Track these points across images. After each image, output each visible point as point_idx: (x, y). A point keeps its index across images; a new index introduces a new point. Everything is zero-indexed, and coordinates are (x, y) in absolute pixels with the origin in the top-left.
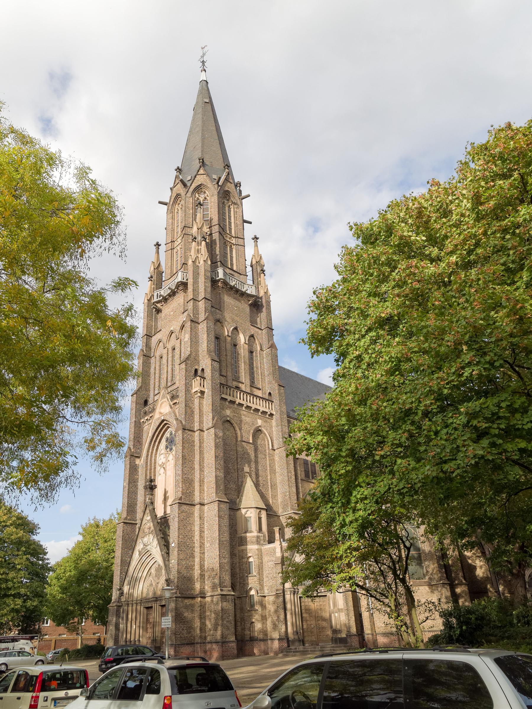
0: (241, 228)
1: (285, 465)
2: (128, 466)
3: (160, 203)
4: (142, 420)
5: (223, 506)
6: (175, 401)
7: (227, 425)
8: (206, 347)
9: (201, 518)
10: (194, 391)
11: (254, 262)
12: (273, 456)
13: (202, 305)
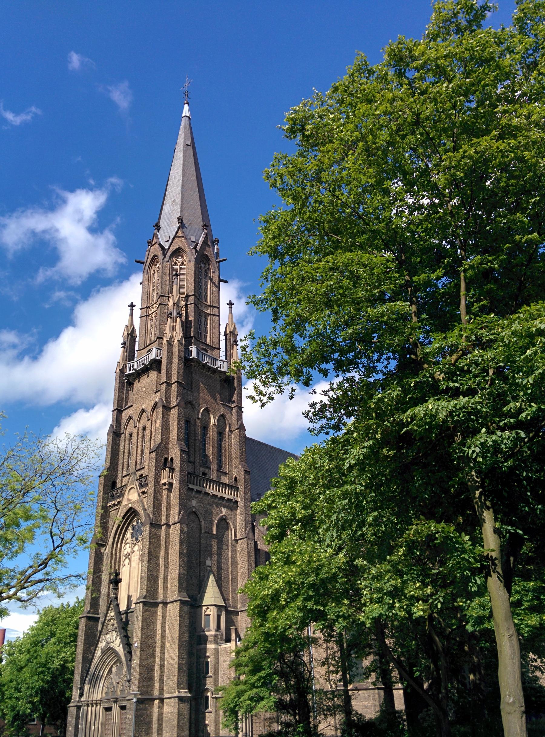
0: (217, 295)
1: (246, 556)
2: (93, 555)
3: (136, 261)
4: (109, 504)
5: (186, 608)
6: (144, 489)
7: (193, 517)
8: (176, 435)
9: (164, 617)
10: (163, 481)
11: (228, 332)
12: (235, 547)
13: (174, 388)
